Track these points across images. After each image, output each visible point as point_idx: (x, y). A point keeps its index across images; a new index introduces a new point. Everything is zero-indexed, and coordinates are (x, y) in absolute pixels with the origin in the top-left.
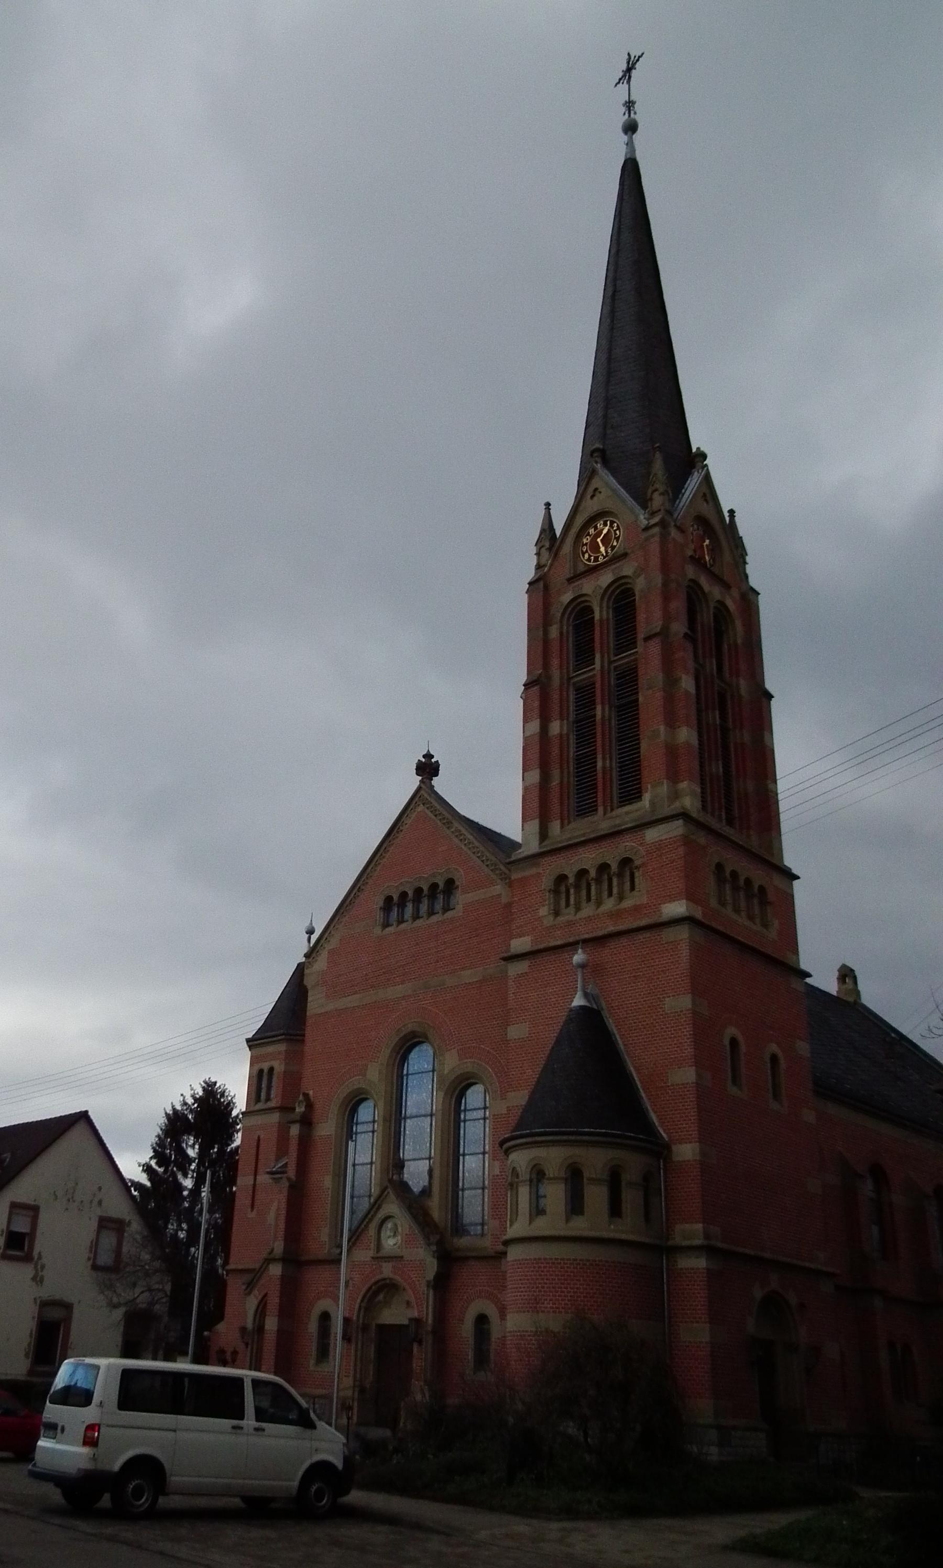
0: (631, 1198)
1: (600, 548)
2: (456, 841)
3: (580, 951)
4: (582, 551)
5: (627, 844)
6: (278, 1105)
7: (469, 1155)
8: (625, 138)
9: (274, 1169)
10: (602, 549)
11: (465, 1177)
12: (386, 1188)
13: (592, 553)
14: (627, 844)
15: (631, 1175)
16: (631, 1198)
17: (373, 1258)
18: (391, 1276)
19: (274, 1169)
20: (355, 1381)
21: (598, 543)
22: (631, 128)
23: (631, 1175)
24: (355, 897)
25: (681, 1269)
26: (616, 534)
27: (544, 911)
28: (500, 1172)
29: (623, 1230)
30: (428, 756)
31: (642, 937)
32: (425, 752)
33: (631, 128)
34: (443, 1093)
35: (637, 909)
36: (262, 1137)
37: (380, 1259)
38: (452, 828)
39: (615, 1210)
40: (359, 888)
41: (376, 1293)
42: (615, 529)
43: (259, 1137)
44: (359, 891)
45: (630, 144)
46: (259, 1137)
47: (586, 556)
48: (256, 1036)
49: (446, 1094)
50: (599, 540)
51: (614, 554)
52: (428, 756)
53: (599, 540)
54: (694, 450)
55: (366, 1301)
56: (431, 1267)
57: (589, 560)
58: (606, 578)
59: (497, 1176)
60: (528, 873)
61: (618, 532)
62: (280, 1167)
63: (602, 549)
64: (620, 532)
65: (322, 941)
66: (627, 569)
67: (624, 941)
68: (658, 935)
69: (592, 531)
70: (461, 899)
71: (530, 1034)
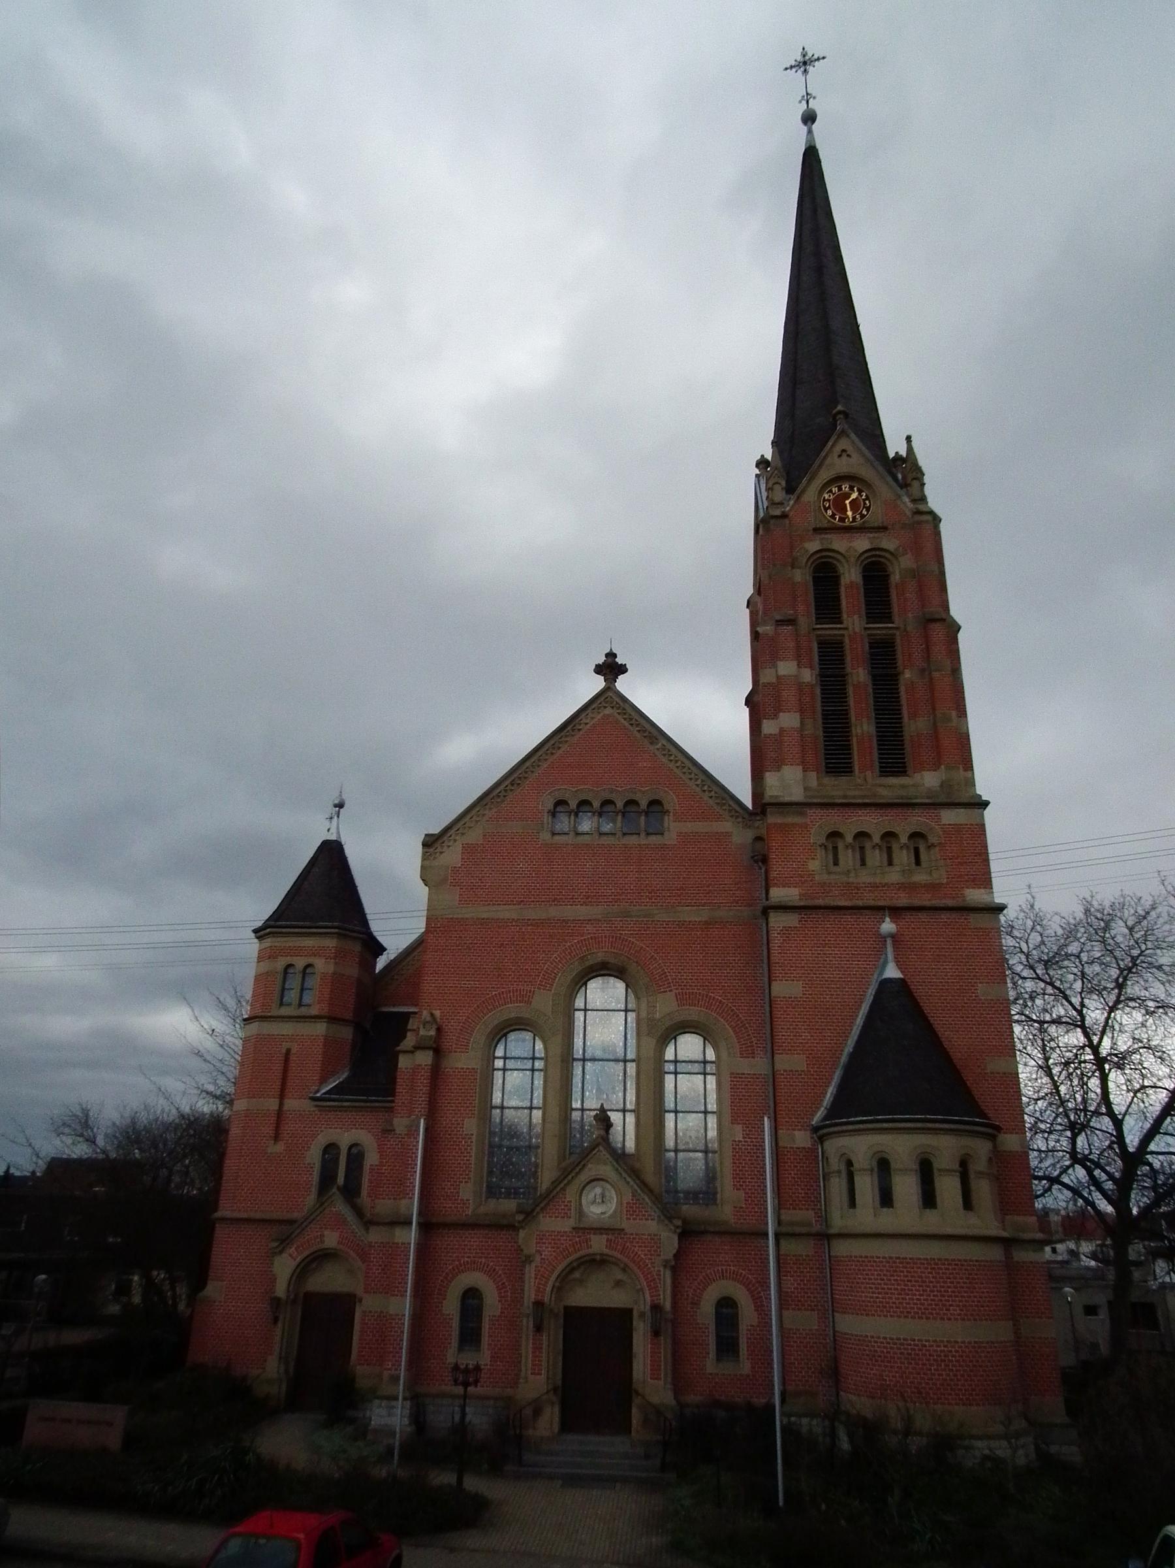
0: (948, 1188)
1: (847, 511)
2: (664, 760)
3: (888, 919)
4: (824, 506)
5: (919, 819)
6: (325, 1012)
7: (682, 1112)
8: (805, 129)
9: (318, 1095)
10: (850, 513)
11: (679, 1137)
12: (597, 1145)
13: (837, 511)
14: (919, 819)
15: (980, 1164)
16: (983, 1190)
17: (574, 1228)
18: (606, 1251)
19: (318, 1095)
20: (548, 1378)
21: (846, 505)
22: (809, 118)
23: (980, 1164)
24: (506, 791)
25: (1018, 1262)
26: (865, 504)
27: (814, 865)
28: (744, 1138)
29: (985, 1222)
30: (611, 655)
31: (944, 916)
32: (608, 651)
33: (809, 118)
34: (655, 1041)
35: (933, 887)
36: (294, 1051)
37: (585, 1230)
38: (657, 744)
39: (929, 1199)
40: (513, 780)
41: (573, 1270)
42: (863, 497)
43: (288, 1051)
44: (512, 785)
45: (810, 132)
46: (288, 1051)
47: (830, 512)
48: (268, 923)
49: (658, 1041)
50: (847, 502)
51: (864, 522)
52: (611, 655)
53: (847, 502)
54: (891, 455)
55: (559, 1280)
56: (670, 1243)
57: (833, 516)
58: (862, 544)
59: (740, 1141)
60: (790, 820)
61: (867, 502)
62: (324, 1094)
63: (850, 513)
64: (870, 502)
65: (452, 832)
66: (888, 543)
67: (923, 916)
68: (965, 919)
69: (835, 490)
70: (674, 829)
71: (804, 994)
